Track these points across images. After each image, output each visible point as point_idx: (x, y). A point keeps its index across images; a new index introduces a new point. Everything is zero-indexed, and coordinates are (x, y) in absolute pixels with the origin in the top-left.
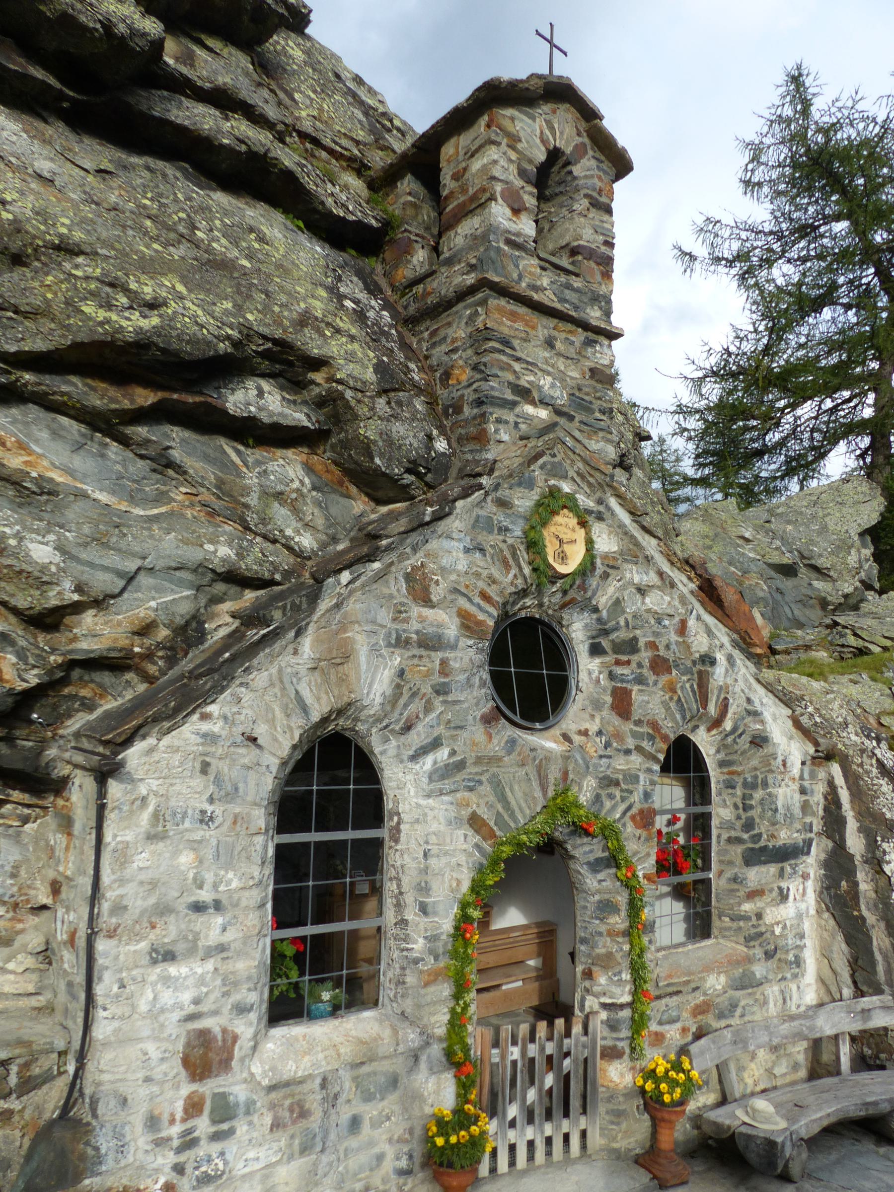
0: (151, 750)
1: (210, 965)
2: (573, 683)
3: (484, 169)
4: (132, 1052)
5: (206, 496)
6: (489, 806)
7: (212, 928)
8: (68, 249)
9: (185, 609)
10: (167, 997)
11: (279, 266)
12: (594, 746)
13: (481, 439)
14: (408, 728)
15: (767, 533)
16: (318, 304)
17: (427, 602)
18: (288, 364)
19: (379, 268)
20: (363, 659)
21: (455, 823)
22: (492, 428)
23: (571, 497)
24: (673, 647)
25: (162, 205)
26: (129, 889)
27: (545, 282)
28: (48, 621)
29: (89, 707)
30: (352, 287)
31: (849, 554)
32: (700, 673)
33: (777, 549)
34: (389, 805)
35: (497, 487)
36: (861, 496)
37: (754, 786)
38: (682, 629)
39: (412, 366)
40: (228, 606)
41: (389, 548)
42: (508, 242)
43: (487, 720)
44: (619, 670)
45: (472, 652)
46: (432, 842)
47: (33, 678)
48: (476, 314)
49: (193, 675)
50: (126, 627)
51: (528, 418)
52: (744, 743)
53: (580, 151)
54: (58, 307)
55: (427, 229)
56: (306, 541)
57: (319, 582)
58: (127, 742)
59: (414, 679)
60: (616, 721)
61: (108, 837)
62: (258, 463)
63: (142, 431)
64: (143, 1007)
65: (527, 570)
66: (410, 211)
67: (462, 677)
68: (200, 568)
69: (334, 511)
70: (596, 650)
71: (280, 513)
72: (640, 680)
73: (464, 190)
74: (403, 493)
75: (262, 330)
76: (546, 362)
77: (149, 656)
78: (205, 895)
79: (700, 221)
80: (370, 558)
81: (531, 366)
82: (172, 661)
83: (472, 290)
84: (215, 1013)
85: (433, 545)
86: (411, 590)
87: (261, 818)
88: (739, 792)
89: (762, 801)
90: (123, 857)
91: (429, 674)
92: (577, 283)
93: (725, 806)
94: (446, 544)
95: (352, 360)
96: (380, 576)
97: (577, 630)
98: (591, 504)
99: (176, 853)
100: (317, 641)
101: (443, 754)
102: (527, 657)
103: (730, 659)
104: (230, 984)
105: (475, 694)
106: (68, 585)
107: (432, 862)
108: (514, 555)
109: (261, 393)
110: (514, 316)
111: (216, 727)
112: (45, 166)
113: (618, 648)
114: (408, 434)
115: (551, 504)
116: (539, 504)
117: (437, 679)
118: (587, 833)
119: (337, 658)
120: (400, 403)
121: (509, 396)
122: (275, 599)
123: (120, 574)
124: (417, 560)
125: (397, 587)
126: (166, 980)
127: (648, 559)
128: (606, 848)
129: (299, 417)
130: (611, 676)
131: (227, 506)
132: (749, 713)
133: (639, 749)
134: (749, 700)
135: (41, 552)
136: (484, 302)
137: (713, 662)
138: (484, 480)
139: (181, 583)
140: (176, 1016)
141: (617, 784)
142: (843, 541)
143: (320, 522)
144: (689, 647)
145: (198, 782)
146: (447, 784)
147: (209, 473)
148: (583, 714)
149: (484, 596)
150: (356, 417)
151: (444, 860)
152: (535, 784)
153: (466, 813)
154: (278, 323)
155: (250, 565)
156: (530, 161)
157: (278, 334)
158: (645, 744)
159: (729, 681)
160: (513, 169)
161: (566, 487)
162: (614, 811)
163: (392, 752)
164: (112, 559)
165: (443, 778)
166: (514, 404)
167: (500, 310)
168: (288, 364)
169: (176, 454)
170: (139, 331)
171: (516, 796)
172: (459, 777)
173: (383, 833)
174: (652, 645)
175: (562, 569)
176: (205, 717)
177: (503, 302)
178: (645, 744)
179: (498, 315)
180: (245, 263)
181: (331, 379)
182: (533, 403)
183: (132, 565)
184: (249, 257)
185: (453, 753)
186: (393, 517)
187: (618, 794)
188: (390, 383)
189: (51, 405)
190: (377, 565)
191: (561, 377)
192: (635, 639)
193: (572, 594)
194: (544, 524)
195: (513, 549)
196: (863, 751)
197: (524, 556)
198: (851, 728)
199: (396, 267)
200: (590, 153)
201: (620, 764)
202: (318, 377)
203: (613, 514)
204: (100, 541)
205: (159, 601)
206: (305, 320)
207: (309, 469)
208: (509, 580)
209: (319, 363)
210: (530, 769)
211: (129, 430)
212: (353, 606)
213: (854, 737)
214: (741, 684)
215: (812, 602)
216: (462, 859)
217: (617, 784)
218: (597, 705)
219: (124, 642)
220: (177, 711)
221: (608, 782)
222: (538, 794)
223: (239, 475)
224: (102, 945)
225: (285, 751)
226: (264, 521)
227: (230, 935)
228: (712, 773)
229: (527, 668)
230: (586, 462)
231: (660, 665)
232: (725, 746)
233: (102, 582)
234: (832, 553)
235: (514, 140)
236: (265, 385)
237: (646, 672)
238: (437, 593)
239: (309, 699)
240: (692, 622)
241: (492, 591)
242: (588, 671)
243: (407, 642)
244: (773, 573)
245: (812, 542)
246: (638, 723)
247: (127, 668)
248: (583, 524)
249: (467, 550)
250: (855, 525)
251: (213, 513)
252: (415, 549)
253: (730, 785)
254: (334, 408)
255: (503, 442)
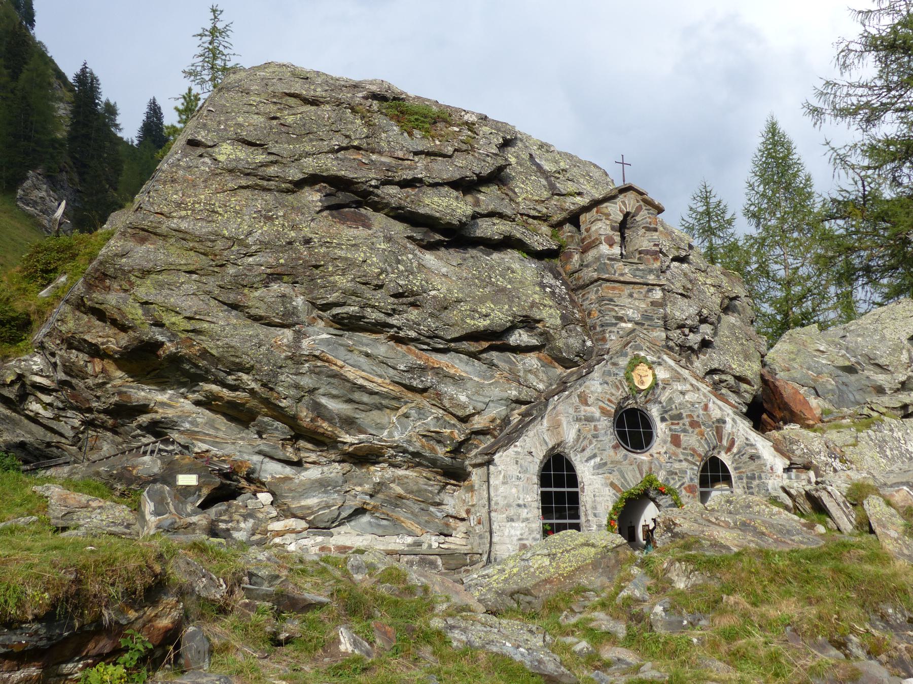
0: (501, 456)
1: (524, 524)
2: (654, 434)
3: (596, 231)
4: (504, 547)
5: (506, 374)
6: (619, 480)
7: (524, 513)
8: (459, 301)
9: (504, 413)
10: (513, 532)
11: (521, 282)
12: (663, 459)
13: (604, 340)
14: (583, 450)
15: (836, 345)
16: (536, 296)
17: (587, 404)
18: (528, 323)
19: (559, 263)
20: (565, 426)
21: (606, 485)
22: (607, 335)
23: (644, 358)
24: (701, 416)
25: (480, 272)
26: (499, 498)
27: (627, 271)
28: (464, 420)
29: (477, 448)
30: (549, 279)
31: (902, 354)
32: (717, 427)
33: (842, 356)
34: (579, 480)
35: (611, 358)
36: (908, 313)
37: (753, 478)
38: (706, 408)
39: (575, 311)
40: (516, 411)
41: (570, 386)
42: (609, 259)
43: (615, 447)
44: (673, 427)
45: (606, 422)
46: (597, 493)
47: (463, 437)
48: (598, 290)
49: (510, 433)
50: (488, 420)
51: (622, 329)
52: (745, 458)
53: (639, 209)
54: (460, 322)
55: (578, 245)
56: (541, 386)
57: (547, 400)
58: (494, 454)
59: (584, 433)
60: (673, 448)
61: (491, 482)
62: (522, 360)
63: (484, 355)
64: (506, 534)
65: (627, 389)
66: (570, 240)
67: (603, 432)
68: (507, 399)
69: (550, 374)
70: (663, 419)
71: (531, 377)
72: (685, 431)
73: (590, 237)
74: (576, 364)
75: (519, 313)
76: (630, 303)
77: (494, 429)
78: (521, 502)
79: (820, 85)
80: (564, 390)
81: (622, 307)
82: (501, 431)
83: (596, 281)
84: (527, 539)
85: (588, 383)
86: (580, 401)
87: (535, 479)
88: (745, 481)
89: (758, 486)
90: (496, 489)
91: (590, 430)
92: (641, 267)
93: (739, 488)
94: (592, 382)
95: (551, 316)
96: (568, 397)
97: (654, 412)
98: (655, 359)
99: (511, 488)
100: (548, 420)
101: (598, 460)
102: (633, 424)
103: (733, 420)
104: (531, 531)
105: (609, 437)
106: (471, 408)
107: (597, 498)
108: (621, 384)
109: (520, 336)
110: (614, 288)
111: (519, 449)
112: (444, 270)
113: (672, 418)
114: (574, 342)
115: (636, 361)
116: (630, 363)
117: (594, 432)
118: (663, 494)
119: (556, 426)
120: (571, 331)
121: (614, 321)
122: (532, 408)
123: (484, 403)
124: (582, 389)
125: (575, 400)
126: (512, 527)
127: (685, 379)
128: (672, 500)
129: (534, 342)
130: (670, 430)
131: (514, 377)
132: (747, 445)
133: (686, 460)
134: (747, 439)
135: (463, 398)
136: (600, 285)
137: (724, 422)
138: (605, 357)
139: (502, 404)
140: (516, 538)
141: (676, 474)
142: (897, 345)
143: (545, 379)
144: (710, 416)
145: (515, 467)
146: (600, 471)
147: (506, 367)
148: (659, 445)
149: (609, 401)
150: (555, 339)
151: (601, 498)
152: (637, 472)
153: (609, 482)
154: (524, 309)
155: (523, 397)
156: (616, 222)
157: (525, 313)
158: (690, 458)
159: (734, 430)
160: (609, 228)
161: (642, 354)
162: (675, 484)
163: (579, 460)
164: (481, 399)
165: (598, 468)
166: (616, 324)
167: (608, 288)
168: (528, 323)
169: (495, 361)
170: (484, 326)
171: (629, 476)
172: (605, 468)
173: (578, 490)
174: (690, 416)
175: (642, 387)
176: (515, 446)
177: (608, 284)
178: (690, 458)
179: (606, 290)
180: (509, 286)
181: (544, 326)
182: (625, 322)
183: (487, 400)
184: (509, 283)
185: (602, 459)
186: (572, 374)
187: (677, 478)
188: (567, 321)
189: (457, 351)
190: (567, 393)
191: (637, 309)
192: (681, 414)
193: (649, 397)
194: (633, 371)
195: (620, 382)
196: (826, 464)
197: (625, 384)
198: (822, 454)
199: (566, 264)
200: (644, 208)
201: (677, 465)
202: (540, 325)
203: (666, 362)
204: (477, 393)
205: (496, 411)
206: (533, 305)
207: (539, 359)
208: (619, 394)
209: (539, 321)
210: (635, 466)
211: (481, 356)
212: (560, 408)
213: (823, 458)
214: (742, 431)
215: (869, 389)
216: (609, 498)
217: (676, 474)
218: (665, 442)
219: (487, 425)
220: (508, 444)
221: (672, 473)
222: (638, 475)
223: (516, 366)
224: (493, 514)
225: (541, 458)
226: (526, 381)
227: (529, 516)
228: (732, 473)
229: (632, 428)
230: (650, 342)
231: (694, 424)
232: (736, 460)
233: (480, 406)
234: (890, 354)
235: (607, 215)
236: (521, 331)
237: (688, 427)
238: (590, 401)
239: (547, 440)
240: (711, 405)
241: (613, 398)
242: (661, 429)
243: (581, 419)
244: (840, 373)
245: (875, 348)
246: (685, 449)
247: (488, 434)
248: (650, 368)
249: (601, 384)
250: (904, 333)
251: (508, 380)
252: (580, 385)
253: (741, 478)
254: (546, 337)
255: (613, 340)
